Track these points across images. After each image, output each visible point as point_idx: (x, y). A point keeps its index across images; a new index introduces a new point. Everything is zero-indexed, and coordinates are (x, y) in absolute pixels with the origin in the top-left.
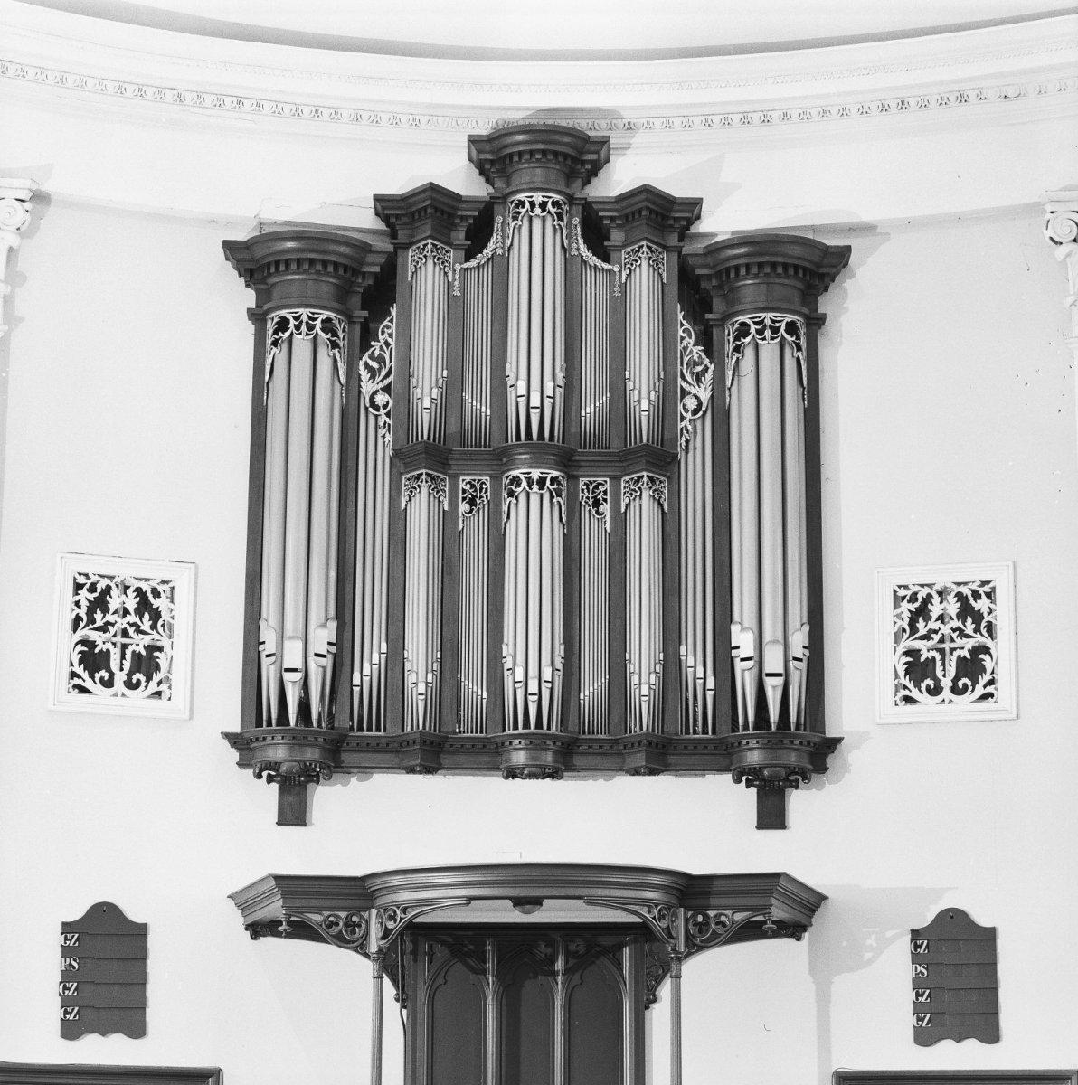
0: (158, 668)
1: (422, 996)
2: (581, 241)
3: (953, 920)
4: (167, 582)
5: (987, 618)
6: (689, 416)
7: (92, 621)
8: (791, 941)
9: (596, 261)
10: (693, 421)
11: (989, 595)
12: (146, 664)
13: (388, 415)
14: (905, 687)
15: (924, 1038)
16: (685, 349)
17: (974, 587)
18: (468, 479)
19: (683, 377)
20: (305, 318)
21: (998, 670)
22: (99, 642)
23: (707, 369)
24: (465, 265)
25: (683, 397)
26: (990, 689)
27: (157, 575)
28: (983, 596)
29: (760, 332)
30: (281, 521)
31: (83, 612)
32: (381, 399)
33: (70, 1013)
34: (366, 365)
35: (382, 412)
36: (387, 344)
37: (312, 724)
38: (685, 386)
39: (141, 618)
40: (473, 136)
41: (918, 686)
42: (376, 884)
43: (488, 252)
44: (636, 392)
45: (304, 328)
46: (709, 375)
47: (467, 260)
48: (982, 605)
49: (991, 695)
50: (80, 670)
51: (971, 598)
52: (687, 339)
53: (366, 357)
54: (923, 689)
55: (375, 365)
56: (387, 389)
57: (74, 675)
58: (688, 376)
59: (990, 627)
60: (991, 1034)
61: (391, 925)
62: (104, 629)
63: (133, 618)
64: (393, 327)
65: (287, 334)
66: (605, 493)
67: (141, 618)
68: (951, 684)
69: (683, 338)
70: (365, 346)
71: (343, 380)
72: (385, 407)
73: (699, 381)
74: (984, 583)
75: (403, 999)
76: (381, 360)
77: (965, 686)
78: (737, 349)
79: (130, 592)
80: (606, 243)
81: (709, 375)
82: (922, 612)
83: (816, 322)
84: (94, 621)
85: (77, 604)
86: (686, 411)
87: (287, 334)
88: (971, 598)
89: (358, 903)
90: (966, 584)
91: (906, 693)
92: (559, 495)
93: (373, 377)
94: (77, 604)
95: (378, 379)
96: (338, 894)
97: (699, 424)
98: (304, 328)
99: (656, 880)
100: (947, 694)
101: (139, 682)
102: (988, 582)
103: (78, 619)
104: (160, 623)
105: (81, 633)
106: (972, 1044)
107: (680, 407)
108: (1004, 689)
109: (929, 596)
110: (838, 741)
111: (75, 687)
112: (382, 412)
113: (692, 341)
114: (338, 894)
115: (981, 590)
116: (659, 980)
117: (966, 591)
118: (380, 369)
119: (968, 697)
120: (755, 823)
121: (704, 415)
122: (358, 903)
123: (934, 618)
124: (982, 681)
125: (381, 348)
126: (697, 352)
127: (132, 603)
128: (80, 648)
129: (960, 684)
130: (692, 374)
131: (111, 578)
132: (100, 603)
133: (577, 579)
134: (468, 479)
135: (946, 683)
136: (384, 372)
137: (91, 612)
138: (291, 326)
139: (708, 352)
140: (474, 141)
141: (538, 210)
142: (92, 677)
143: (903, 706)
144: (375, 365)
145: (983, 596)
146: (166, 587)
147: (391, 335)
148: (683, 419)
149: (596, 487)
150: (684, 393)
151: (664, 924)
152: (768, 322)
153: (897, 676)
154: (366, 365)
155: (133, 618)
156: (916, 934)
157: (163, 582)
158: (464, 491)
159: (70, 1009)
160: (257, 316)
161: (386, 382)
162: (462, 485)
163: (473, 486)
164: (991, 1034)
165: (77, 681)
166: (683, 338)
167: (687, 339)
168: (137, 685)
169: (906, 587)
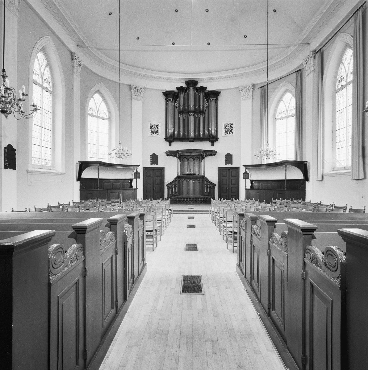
60: (232, 164)
82: (227, 126)
108: (233, 133)
119: (231, 134)
156: (225, 155)
164: (232, 164)
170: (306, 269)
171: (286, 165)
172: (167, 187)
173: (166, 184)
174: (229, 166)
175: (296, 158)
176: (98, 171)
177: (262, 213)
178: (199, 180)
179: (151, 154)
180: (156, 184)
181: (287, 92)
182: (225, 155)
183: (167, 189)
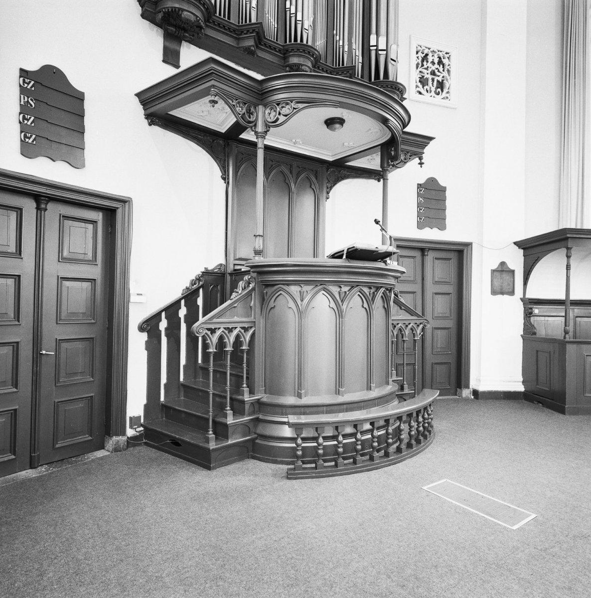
3: (432, 181)
7: (423, 65)
11: (448, 58)
12: (441, 85)
15: (420, 226)
26: (448, 95)
30: (389, 11)
33: (29, 138)
48: (445, 61)
50: (419, 84)
57: (417, 86)
59: (448, 71)
60: (442, 227)
62: (427, 69)
82: (425, 58)
100: (433, 94)
101: (439, 91)
103: (418, 65)
105: (420, 69)
106: (435, 230)
108: (452, 96)
119: (440, 97)
127: (436, 60)
131: (429, 49)
132: (425, 58)
133: (279, 6)
137: (423, 61)
142: (423, 87)
146: (448, 55)
155: (436, 66)
156: (419, 186)
157: (447, 53)
159: (29, 135)
164: (442, 227)
165: (418, 89)
168: (438, 94)
170: (364, 424)
171: (568, 249)
172: (144, 336)
173: (137, 315)
174: (431, 234)
175: (576, 225)
176: (568, 267)
177: (235, 304)
178: (335, 289)
179: (33, 66)
180: (62, 259)
181: (102, 212)
182: (419, 186)
183: (145, 354)
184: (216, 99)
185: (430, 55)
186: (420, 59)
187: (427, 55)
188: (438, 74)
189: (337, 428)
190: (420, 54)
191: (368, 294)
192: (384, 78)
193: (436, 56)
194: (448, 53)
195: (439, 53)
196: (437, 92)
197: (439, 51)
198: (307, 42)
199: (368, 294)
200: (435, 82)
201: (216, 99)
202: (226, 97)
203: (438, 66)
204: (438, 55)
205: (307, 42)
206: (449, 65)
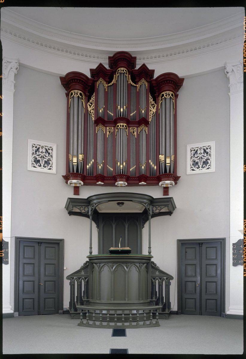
0: (50, 164)
1: (102, 228)
2: (131, 80)
4: (51, 147)
5: (210, 153)
6: (151, 115)
8: (169, 216)
9: (133, 84)
10: (152, 116)
13: (93, 114)
14: (192, 167)
16: (151, 102)
17: (207, 147)
18: (109, 127)
19: (150, 107)
20: (76, 92)
21: (212, 163)
22: (38, 158)
23: (155, 106)
24: (108, 85)
25: (150, 111)
27: (49, 146)
28: (209, 149)
29: (166, 95)
31: (34, 152)
32: (92, 111)
34: (89, 104)
35: (92, 114)
36: (93, 100)
37: (79, 171)
38: (151, 109)
39: (46, 154)
40: (128, 350)
41: (195, 167)
42: (90, 199)
43: (112, 83)
44: (141, 109)
45: (76, 94)
46: (155, 107)
47: (108, 84)
49: (210, 168)
51: (206, 149)
52: (151, 100)
53: (89, 103)
54: (196, 167)
55: (90, 104)
56: (93, 109)
58: (151, 107)
61: (93, 208)
63: (44, 154)
64: (94, 97)
65: (72, 96)
66: (135, 130)
67: (46, 154)
68: (201, 166)
69: (150, 100)
70: (89, 101)
71: (84, 107)
72: (93, 113)
73: (154, 108)
74: (208, 146)
75: (98, 227)
76: (92, 103)
77: (204, 166)
78: (161, 100)
79: (44, 149)
80: (136, 80)
81: (155, 107)
83: (176, 96)
84: (37, 154)
85: (33, 150)
86: (151, 114)
87: (72, 96)
88: (206, 149)
89: (87, 205)
90: (205, 147)
91: (192, 168)
92: (126, 129)
93: (90, 107)
94: (33, 150)
95: (91, 107)
96: (83, 202)
97: (153, 117)
98: (76, 94)
99: (147, 197)
100: (42, 167)
101: (46, 166)
102: (209, 146)
104: (50, 155)
105: (34, 156)
107: (150, 114)
109: (198, 150)
110: (180, 177)
111: (33, 166)
112: (92, 114)
113: (152, 100)
114: (83, 202)
115: (208, 148)
116: (144, 223)
117: (205, 148)
118: (92, 105)
119: (205, 168)
120: (163, 194)
121: (154, 115)
122: (87, 205)
123: (198, 154)
124: (208, 165)
125: (92, 101)
126: (153, 102)
128: (34, 159)
129: (203, 166)
130: (152, 107)
134: (109, 127)
135: (201, 166)
136: (92, 106)
137: (36, 151)
138: (73, 94)
139: (156, 103)
140: (110, 58)
141: (122, 127)
142: (37, 165)
143: (192, 171)
144: (90, 104)
145: (209, 149)
146: (209, 147)
147: (94, 99)
148: (150, 115)
149: (134, 129)
150: (151, 111)
151: (148, 207)
152: (168, 93)
153: (191, 165)
154: (89, 104)
158: (108, 130)
160: (67, 95)
161: (93, 108)
162: (108, 129)
163: (110, 129)
166: (150, 100)
167: (151, 100)
168: (45, 167)
169: (193, 148)
184: (70, 93)
185: (41, 148)
186: (34, 150)
187: (38, 149)
188: (203, 158)
189: (144, 311)
190: (34, 148)
191: (139, 267)
192: (164, 173)
193: (44, 149)
194: (209, 146)
195: (46, 147)
196: (45, 166)
197: (203, 147)
198: (125, 174)
199: (139, 267)
200: (44, 161)
201: (70, 93)
202: (77, 86)
203: (203, 154)
204: (45, 148)
205: (125, 174)
206: (210, 151)
